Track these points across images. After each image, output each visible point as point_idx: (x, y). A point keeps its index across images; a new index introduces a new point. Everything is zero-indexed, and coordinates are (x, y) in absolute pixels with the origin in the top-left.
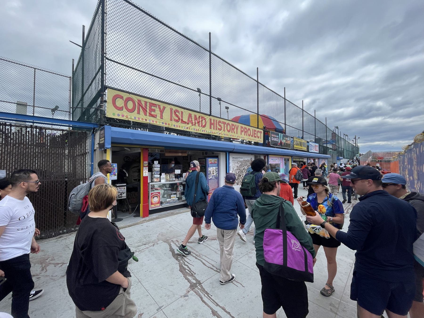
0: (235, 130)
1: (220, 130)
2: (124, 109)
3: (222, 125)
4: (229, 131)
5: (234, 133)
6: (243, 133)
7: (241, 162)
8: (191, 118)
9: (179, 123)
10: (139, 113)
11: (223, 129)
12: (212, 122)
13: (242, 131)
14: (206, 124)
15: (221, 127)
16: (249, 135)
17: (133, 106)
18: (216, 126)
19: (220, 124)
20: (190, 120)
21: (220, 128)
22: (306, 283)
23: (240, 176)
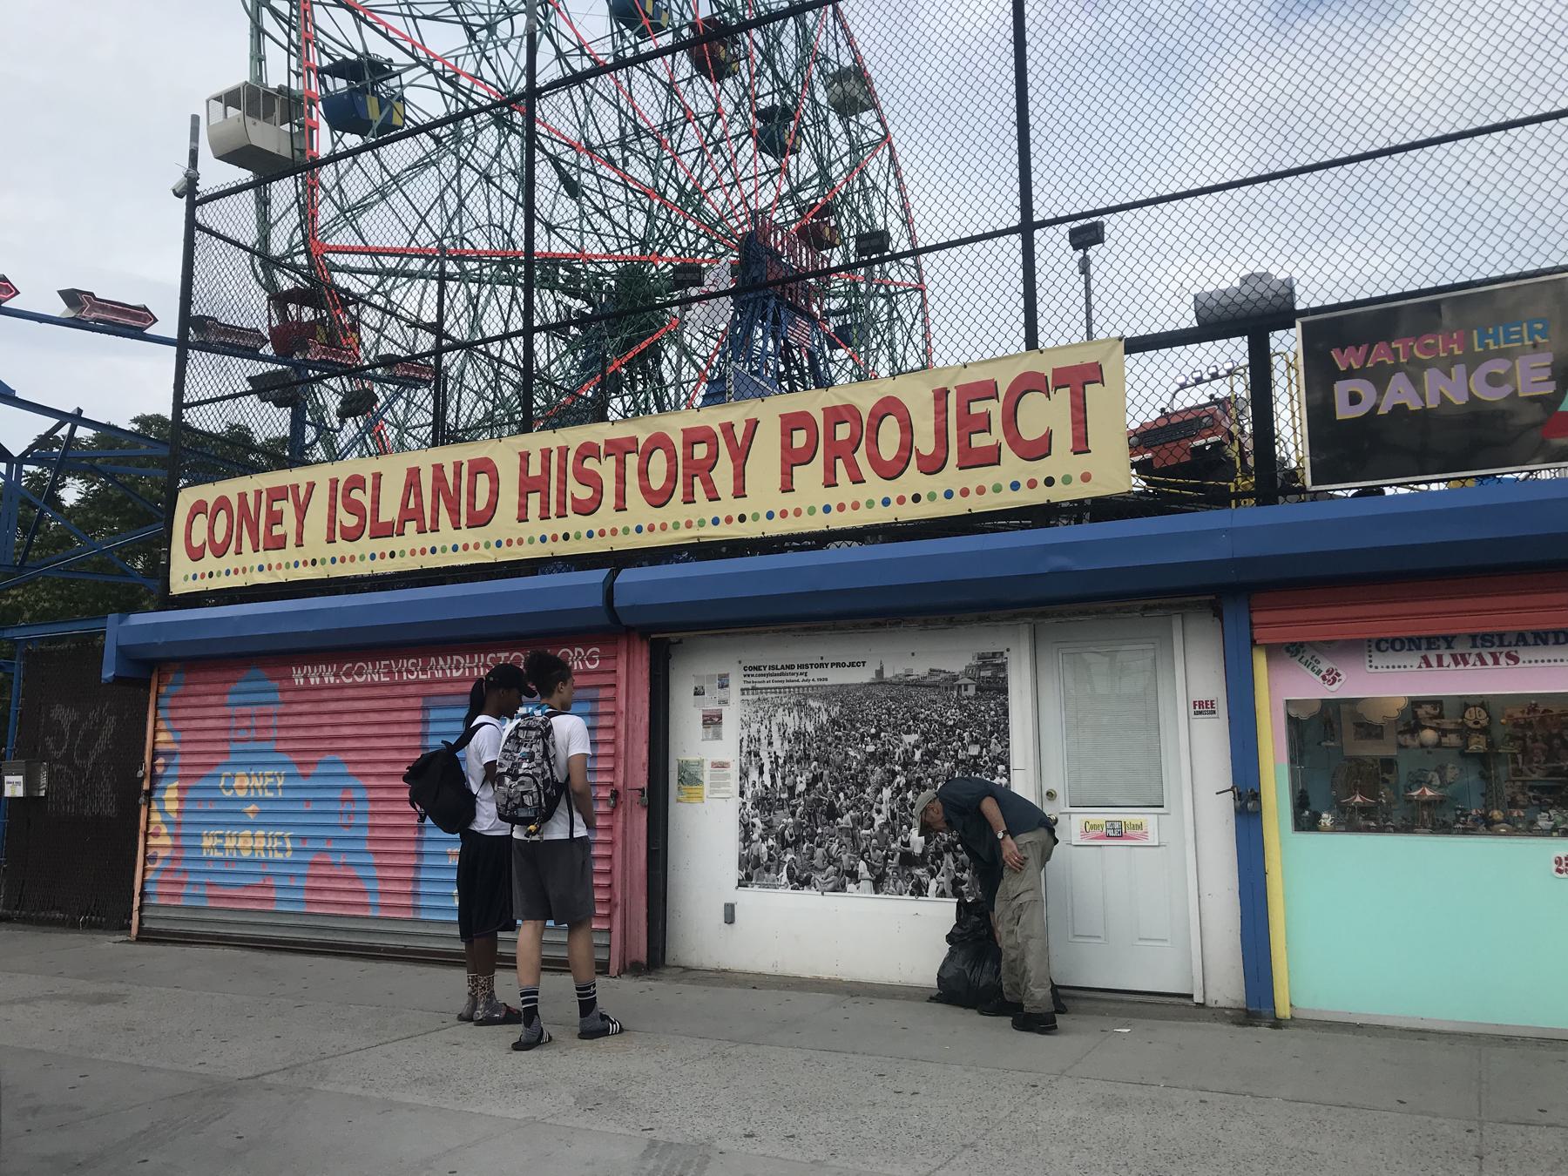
0: (723, 474)
1: (587, 509)
2: (1007, 453)
3: (606, 469)
4: (658, 499)
5: (713, 497)
6: (809, 476)
7: (830, 694)
8: (419, 495)
9: (366, 544)
10: (689, 499)
11: (609, 499)
12: (535, 470)
13: (792, 459)
14: (492, 506)
15: (599, 492)
16: (891, 472)
17: (902, 446)
18: (562, 492)
19: (590, 464)
20: (412, 505)
21: (585, 493)
22: (1561, 409)
23: (833, 813)
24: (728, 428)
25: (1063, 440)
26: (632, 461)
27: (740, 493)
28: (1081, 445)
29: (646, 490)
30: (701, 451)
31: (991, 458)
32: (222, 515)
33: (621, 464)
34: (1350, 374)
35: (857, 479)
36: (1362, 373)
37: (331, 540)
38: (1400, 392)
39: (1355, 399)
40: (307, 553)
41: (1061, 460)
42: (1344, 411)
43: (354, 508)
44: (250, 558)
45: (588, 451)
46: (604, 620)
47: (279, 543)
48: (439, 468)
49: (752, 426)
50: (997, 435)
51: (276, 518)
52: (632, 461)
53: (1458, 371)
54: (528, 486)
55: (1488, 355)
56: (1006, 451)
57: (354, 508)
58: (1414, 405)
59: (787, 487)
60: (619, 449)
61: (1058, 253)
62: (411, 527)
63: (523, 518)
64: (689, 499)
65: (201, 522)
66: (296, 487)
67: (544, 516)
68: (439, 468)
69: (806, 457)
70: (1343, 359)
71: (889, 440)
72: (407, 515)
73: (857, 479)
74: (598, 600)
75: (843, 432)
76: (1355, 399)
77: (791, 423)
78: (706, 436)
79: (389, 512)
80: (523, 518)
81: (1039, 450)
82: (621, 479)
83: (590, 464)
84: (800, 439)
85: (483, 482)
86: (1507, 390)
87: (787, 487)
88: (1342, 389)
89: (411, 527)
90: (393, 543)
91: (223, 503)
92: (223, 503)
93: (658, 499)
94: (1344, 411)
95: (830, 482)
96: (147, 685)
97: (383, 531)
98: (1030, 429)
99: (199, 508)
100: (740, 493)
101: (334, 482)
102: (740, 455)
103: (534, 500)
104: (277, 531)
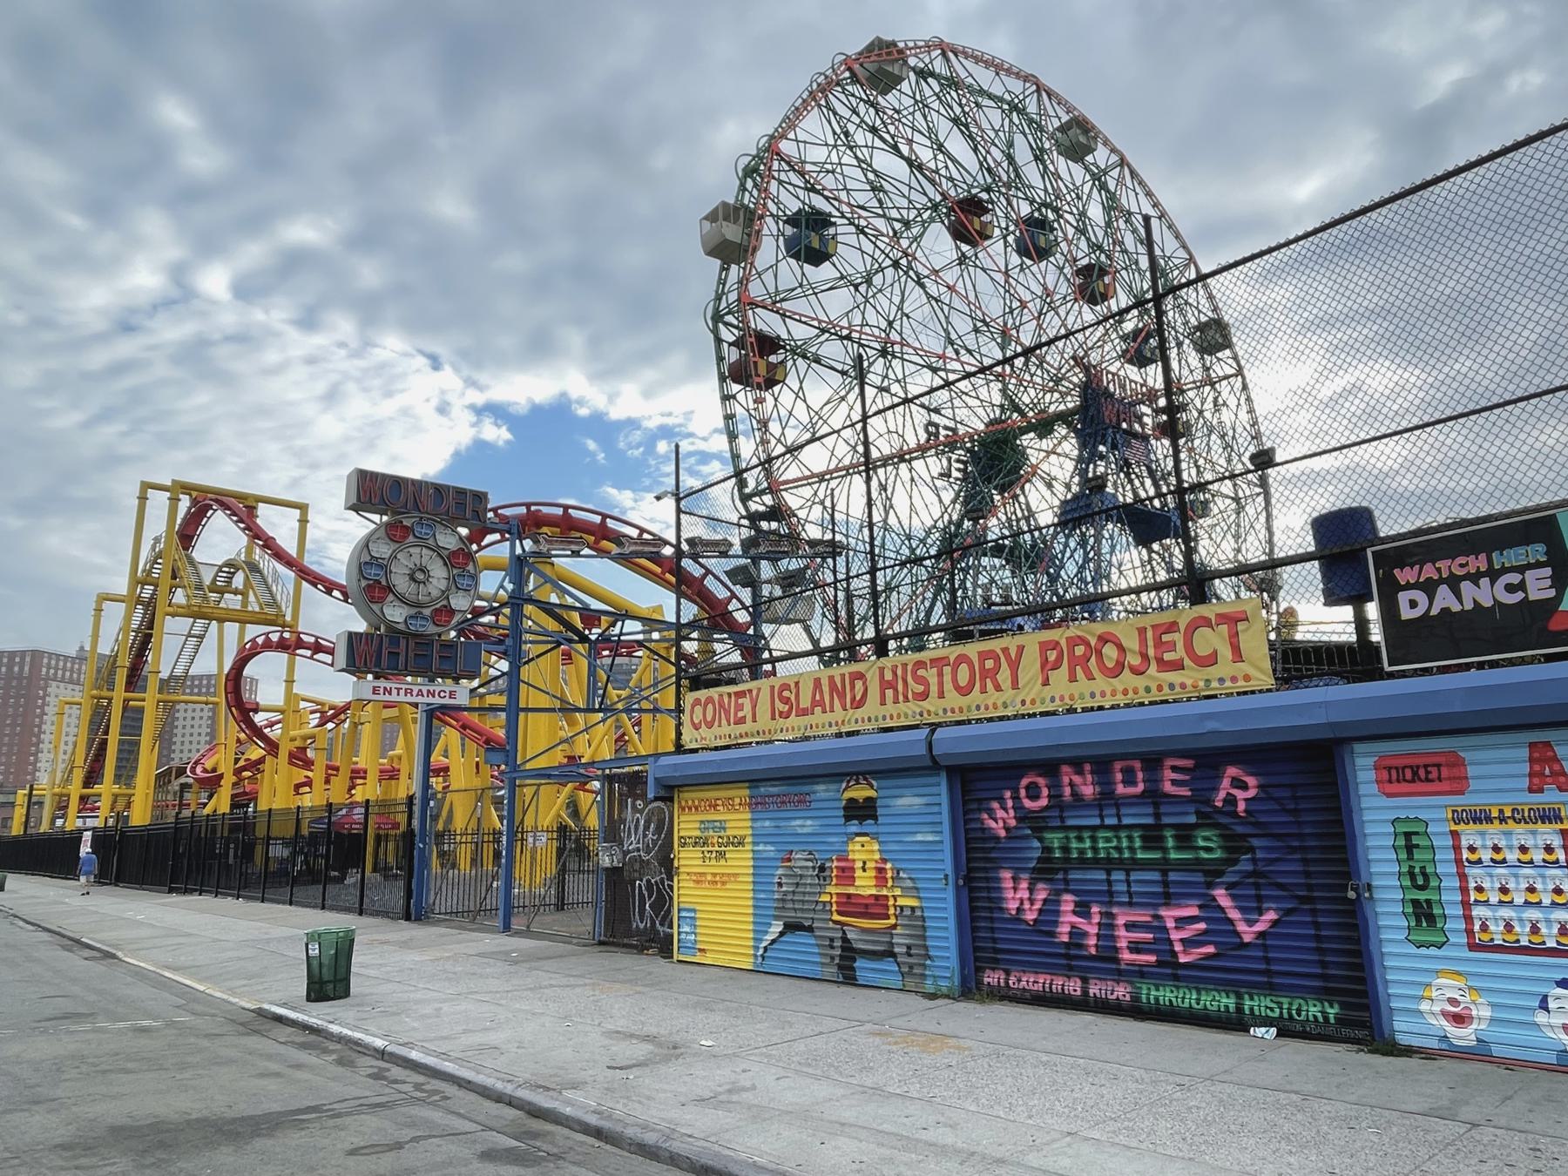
0: (1004, 676)
3: (931, 675)
5: (998, 688)
6: (1060, 676)
9: (793, 720)
10: (983, 691)
12: (888, 676)
19: (921, 672)
24: (1005, 650)
25: (1225, 652)
26: (947, 670)
27: (1015, 685)
28: (1238, 655)
29: (958, 688)
30: (989, 664)
31: (1178, 666)
32: (710, 706)
33: (940, 675)
34: (1408, 587)
35: (1091, 677)
36: (1415, 586)
37: (773, 718)
38: (1445, 598)
39: (1413, 604)
40: (759, 726)
41: (1225, 667)
42: (1407, 614)
43: (787, 701)
44: (726, 729)
45: (920, 664)
46: (929, 763)
47: (742, 721)
48: (831, 678)
49: (1021, 649)
50: (1180, 653)
51: (740, 707)
52: (947, 670)
53: (1485, 582)
54: (885, 685)
55: (1505, 570)
56: (1187, 662)
57: (787, 701)
58: (1456, 607)
59: (1046, 683)
60: (939, 663)
61: (1382, 506)
62: (818, 710)
63: (883, 703)
64: (983, 691)
65: (698, 709)
66: (750, 691)
67: (896, 701)
68: (831, 678)
69: (1057, 666)
70: (1404, 575)
71: (1110, 652)
72: (814, 704)
73: (1091, 677)
74: (922, 750)
75: (1079, 650)
76: (1413, 604)
77: (1045, 647)
78: (991, 654)
79: (805, 702)
80: (883, 703)
81: (1212, 660)
82: (941, 684)
83: (921, 672)
84: (1052, 656)
85: (859, 684)
86: (1520, 596)
87: (1046, 683)
88: (1403, 598)
89: (818, 710)
90: (807, 720)
91: (710, 700)
92: (710, 700)
93: (965, 691)
94: (1407, 614)
95: (1073, 678)
96: (671, 800)
97: (803, 712)
98: (1202, 650)
99: (697, 702)
100: (1015, 685)
101: (772, 688)
102: (1014, 666)
103: (889, 693)
104: (740, 714)
